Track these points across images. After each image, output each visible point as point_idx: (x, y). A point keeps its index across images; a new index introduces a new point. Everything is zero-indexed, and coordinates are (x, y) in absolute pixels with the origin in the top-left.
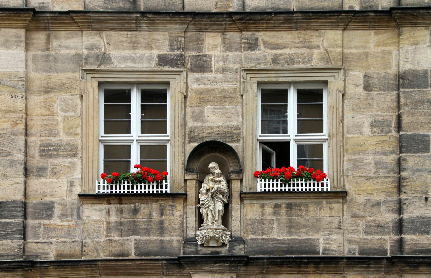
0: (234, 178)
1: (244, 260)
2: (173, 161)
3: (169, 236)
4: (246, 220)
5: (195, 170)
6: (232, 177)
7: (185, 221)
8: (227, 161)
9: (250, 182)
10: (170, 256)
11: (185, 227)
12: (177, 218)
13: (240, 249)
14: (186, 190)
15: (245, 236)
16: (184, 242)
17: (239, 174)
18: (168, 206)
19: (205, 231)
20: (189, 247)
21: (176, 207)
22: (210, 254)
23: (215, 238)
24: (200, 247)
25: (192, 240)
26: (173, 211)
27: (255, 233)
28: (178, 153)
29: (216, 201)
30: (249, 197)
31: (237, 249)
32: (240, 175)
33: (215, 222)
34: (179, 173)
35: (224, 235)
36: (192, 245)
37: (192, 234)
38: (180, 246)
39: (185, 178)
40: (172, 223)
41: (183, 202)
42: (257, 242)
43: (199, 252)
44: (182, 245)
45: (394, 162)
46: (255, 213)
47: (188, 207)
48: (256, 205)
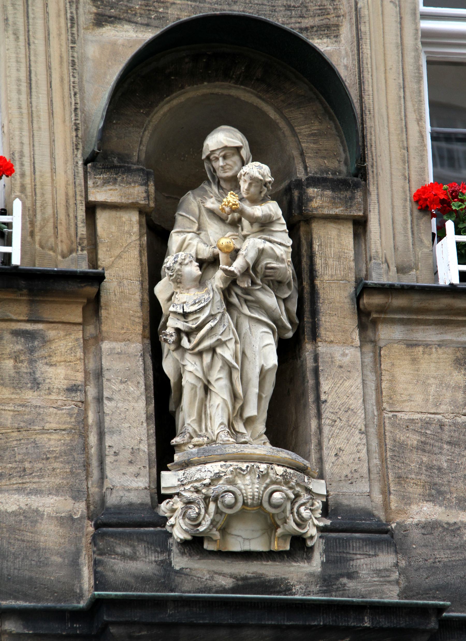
0: (326, 211)
1: (424, 631)
2: (25, 111)
3: (18, 491)
4: (393, 425)
5: (135, 159)
6: (314, 204)
7: (91, 418)
8: (282, 124)
9: (400, 238)
10: (25, 597)
11: (93, 451)
12: (53, 397)
13: (378, 572)
14: (94, 262)
15: (393, 505)
16: (97, 526)
17: (348, 194)
18: (7, 337)
19: (215, 467)
20: (128, 550)
21: (46, 341)
22: (234, 590)
23: (266, 505)
24: (183, 554)
25: (137, 517)
26: (32, 362)
27: (440, 493)
28: (49, 68)
29: (245, 324)
30: (402, 310)
31: (363, 573)
32: (352, 198)
33: (240, 427)
34: (53, 171)
35: (305, 497)
36: (140, 540)
37: (134, 485)
38: (73, 548)
39: (92, 198)
40: (31, 422)
41: (80, 320)
42: (456, 540)
43: (178, 580)
44: (86, 541)
45: (346, 301)
46: (432, 390)
47: (106, 346)
48: (436, 354)
